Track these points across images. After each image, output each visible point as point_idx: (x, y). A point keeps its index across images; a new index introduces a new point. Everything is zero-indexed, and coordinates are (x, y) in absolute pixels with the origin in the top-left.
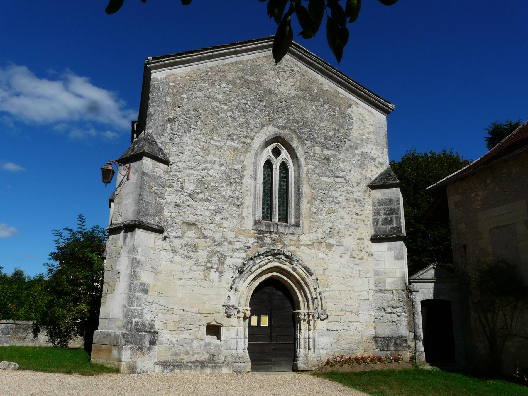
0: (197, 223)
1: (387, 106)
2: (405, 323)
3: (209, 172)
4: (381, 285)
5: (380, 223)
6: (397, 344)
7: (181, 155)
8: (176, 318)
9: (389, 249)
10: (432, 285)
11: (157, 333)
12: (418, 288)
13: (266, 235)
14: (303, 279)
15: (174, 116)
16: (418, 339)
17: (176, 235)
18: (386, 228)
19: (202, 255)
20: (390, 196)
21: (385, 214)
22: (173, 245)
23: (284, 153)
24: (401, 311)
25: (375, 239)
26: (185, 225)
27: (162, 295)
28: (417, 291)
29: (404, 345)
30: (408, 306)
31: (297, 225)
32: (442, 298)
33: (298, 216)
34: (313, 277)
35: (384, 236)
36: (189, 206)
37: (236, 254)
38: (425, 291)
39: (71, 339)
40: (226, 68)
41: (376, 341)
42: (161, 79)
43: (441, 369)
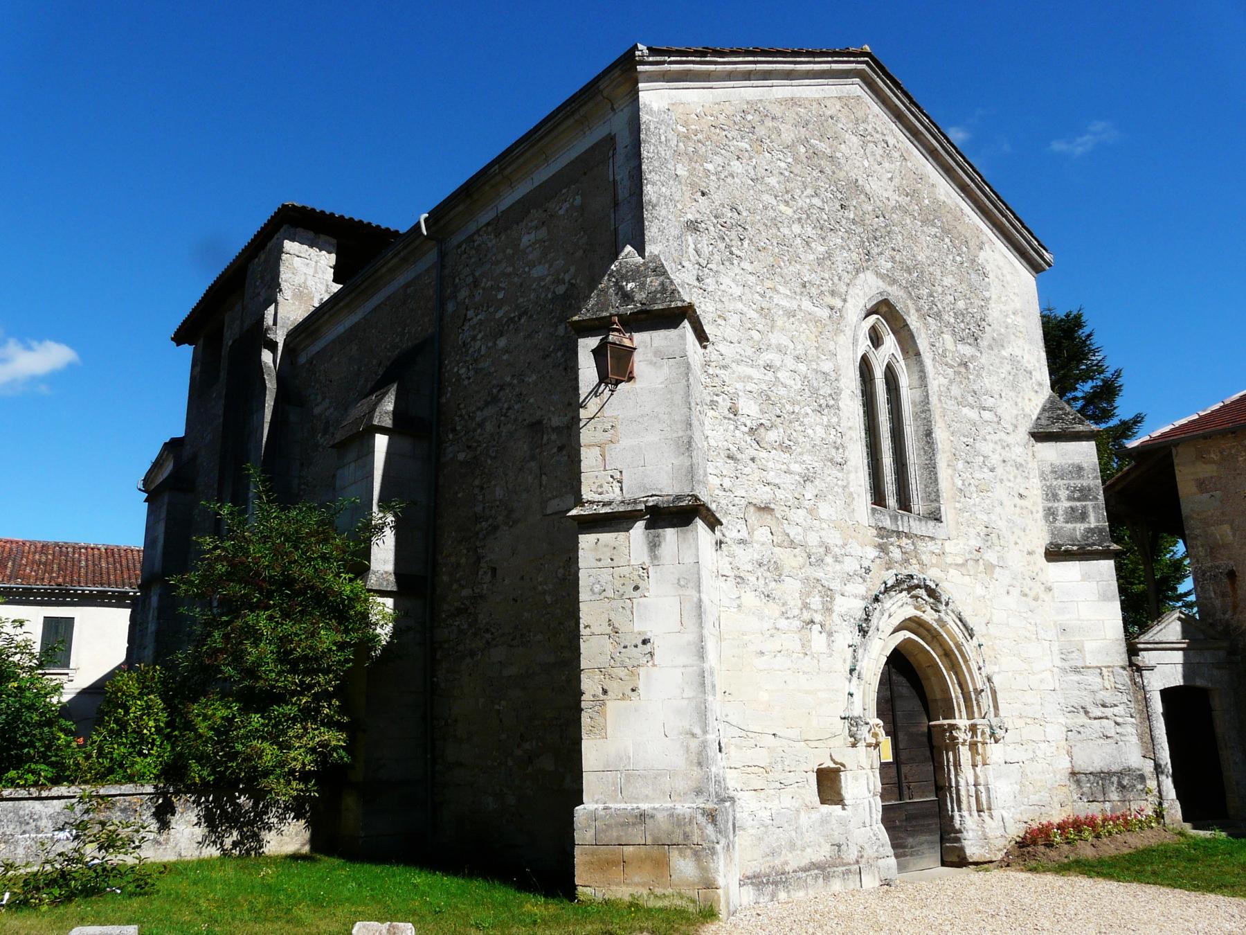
0: (772, 506)
1: (1042, 257)
2: (1134, 739)
3: (779, 375)
4: (1074, 655)
5: (1061, 518)
6: (1124, 787)
7: (723, 323)
8: (762, 758)
9: (1086, 577)
10: (1178, 657)
11: (732, 799)
12: (1153, 663)
13: (892, 540)
14: (959, 646)
15: (698, 216)
16: (1162, 773)
17: (739, 536)
18: (1074, 529)
19: (791, 588)
20: (1077, 460)
21: (1070, 499)
22: (736, 563)
23: (890, 341)
24: (1123, 713)
25: (1055, 554)
26: (752, 509)
27: (730, 698)
28: (1151, 669)
29: (1140, 787)
30: (1137, 701)
31: (936, 517)
32: (1199, 683)
33: (933, 496)
34: (975, 642)
35: (1075, 548)
36: (753, 460)
37: (850, 588)
38: (1167, 669)
39: (270, 829)
40: (777, 110)
41: (1078, 782)
42: (659, 111)
43: (1229, 835)
